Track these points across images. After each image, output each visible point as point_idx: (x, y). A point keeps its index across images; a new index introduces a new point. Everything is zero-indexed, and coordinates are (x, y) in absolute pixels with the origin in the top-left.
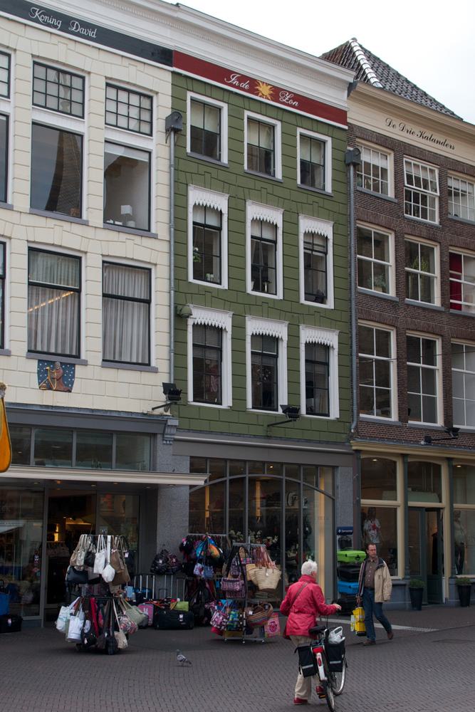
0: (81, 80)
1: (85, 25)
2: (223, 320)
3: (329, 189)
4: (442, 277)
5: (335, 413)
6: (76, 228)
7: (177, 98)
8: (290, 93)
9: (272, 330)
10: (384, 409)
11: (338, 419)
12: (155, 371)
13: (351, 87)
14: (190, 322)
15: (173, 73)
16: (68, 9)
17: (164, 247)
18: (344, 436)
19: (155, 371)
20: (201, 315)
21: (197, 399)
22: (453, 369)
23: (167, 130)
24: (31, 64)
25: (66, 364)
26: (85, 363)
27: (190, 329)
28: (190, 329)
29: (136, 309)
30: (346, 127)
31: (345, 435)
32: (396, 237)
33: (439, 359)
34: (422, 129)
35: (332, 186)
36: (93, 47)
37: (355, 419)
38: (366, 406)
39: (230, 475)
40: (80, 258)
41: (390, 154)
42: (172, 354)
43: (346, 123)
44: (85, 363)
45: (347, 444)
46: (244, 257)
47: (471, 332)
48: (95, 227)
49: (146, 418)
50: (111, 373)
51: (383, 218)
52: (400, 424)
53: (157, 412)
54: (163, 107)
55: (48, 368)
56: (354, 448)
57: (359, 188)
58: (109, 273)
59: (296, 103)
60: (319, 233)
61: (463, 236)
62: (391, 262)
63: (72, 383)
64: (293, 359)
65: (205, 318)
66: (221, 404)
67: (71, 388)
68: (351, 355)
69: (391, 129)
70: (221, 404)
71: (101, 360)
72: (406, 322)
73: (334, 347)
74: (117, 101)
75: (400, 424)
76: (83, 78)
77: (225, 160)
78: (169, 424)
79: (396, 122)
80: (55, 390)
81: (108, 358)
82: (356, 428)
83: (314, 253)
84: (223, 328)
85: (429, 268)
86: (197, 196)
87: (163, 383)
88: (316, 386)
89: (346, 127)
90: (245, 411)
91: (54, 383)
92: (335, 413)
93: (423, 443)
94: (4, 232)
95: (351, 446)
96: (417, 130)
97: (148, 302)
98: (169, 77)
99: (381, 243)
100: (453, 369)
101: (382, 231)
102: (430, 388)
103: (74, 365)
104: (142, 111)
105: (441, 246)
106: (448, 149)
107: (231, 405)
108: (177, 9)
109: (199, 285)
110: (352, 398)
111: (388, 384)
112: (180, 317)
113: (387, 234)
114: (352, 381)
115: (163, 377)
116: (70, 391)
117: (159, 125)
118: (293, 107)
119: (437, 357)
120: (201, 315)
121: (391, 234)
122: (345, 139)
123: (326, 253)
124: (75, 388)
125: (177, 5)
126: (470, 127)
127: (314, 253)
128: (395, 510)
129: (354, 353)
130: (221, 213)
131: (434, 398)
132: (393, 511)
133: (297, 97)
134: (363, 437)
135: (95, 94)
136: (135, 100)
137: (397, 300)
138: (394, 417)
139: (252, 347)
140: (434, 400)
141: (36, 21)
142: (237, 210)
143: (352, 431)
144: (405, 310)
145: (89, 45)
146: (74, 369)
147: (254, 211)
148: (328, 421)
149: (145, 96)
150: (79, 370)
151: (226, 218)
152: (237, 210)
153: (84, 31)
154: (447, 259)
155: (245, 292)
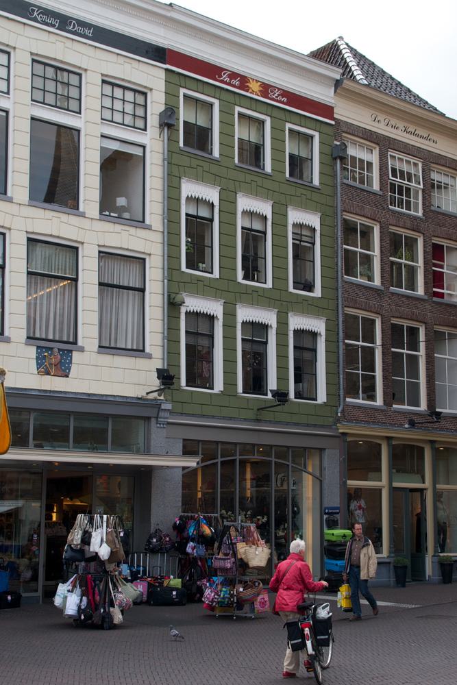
0: (78, 77)
1: (82, 24)
2: (214, 307)
3: (316, 182)
4: (425, 267)
5: (322, 397)
6: (74, 220)
7: (171, 94)
8: (279, 89)
9: (262, 318)
10: (370, 393)
11: (325, 403)
12: (149, 357)
13: (338, 84)
14: (183, 310)
15: (167, 70)
16: (66, 9)
17: (158, 238)
18: (331, 419)
19: (149, 357)
20: (193, 303)
21: (190, 384)
22: (436, 355)
23: (161, 126)
24: (30, 62)
25: (63, 350)
26: (82, 350)
27: (183, 317)
28: (183, 317)
29: (131, 298)
30: (333, 123)
31: (332, 419)
32: (381, 228)
33: (422, 346)
34: (406, 125)
35: (320, 179)
37: (342, 403)
38: (352, 391)
39: (221, 457)
40: (77, 248)
41: (375, 148)
42: (166, 340)
43: (333, 119)
44: (82, 350)
45: (334, 427)
46: (235, 247)
47: (453, 319)
48: (92, 219)
49: (140, 402)
50: (107, 359)
51: (368, 210)
52: (385, 408)
53: (151, 396)
54: (157, 103)
55: (46, 354)
56: (341, 431)
57: (345, 181)
58: (105, 262)
59: (285, 99)
60: (307, 224)
61: (445, 227)
62: (376, 252)
63: (69, 368)
64: (282, 346)
65: (197, 306)
66: (212, 389)
67: (69, 374)
68: (338, 342)
69: (376, 124)
70: (212, 389)
71: (97, 346)
73: (322, 334)
74: (113, 98)
75: (385, 408)
76: (80, 75)
77: (216, 154)
78: (163, 407)
79: (381, 117)
80: (53, 375)
81: (104, 344)
82: (343, 412)
83: (302, 243)
84: (215, 316)
85: (413, 257)
86: (189, 188)
87: (157, 369)
88: (304, 371)
89: (333, 123)
90: (235, 395)
91: (52, 369)
92: (322, 397)
93: (406, 426)
94: (4, 223)
95: (338, 429)
96: (401, 125)
97: (143, 290)
98: (162, 74)
99: (366, 233)
100: (436, 355)
101: (367, 222)
102: (414, 373)
103: (71, 351)
104: (137, 107)
105: (424, 236)
106: (431, 143)
107: (222, 390)
108: (170, 8)
109: (191, 274)
110: (339, 383)
111: (373, 369)
112: (173, 305)
113: (373, 225)
114: (338, 366)
115: (157, 363)
116: (67, 377)
117: (153, 121)
118: (282, 103)
119: (421, 343)
120: (193, 303)
121: (376, 225)
123: (314, 244)
124: (73, 373)
125: (171, 5)
126: (452, 123)
127: (302, 243)
128: (380, 491)
129: (341, 340)
130: (212, 205)
131: (418, 383)
132: (378, 491)
133: (285, 93)
135: (92, 91)
136: (129, 96)
138: (379, 401)
139: (243, 334)
140: (417, 385)
141: (35, 20)
142: (228, 202)
143: (339, 414)
144: (390, 298)
146: (72, 355)
147: (245, 203)
148: (316, 405)
149: (140, 92)
150: (76, 356)
151: (218, 210)
152: (228, 202)
153: (80, 30)
154: (430, 249)
155: (235, 281)
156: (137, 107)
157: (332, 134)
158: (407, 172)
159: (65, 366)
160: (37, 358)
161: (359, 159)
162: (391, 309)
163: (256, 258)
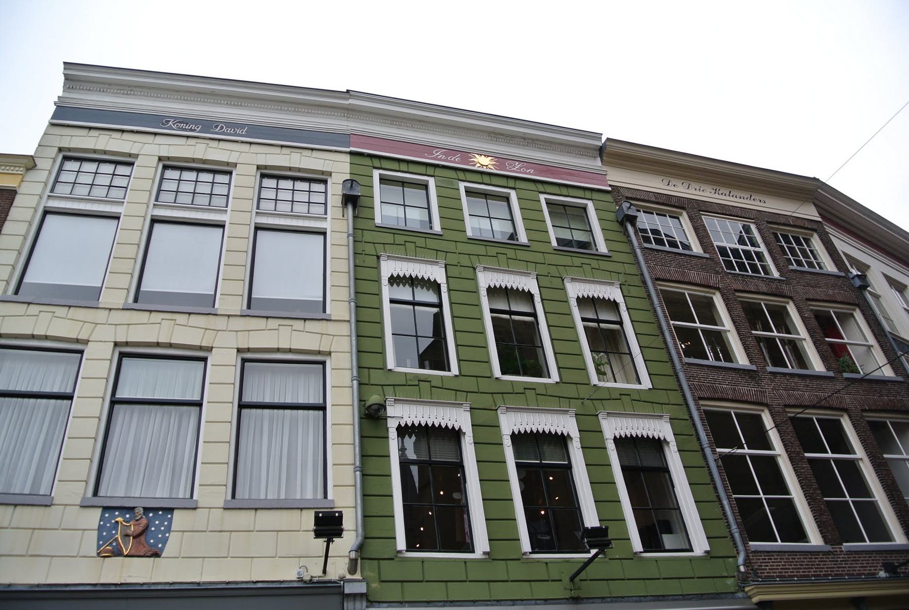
4: (812, 337)
5: (700, 545)
9: (635, 428)
11: (707, 552)
14: (392, 425)
15: (352, 153)
17: (345, 329)
18: (730, 581)
21: (536, 550)
22: (885, 456)
28: (393, 434)
30: (610, 189)
31: (732, 579)
32: (722, 296)
33: (774, 436)
36: (242, 142)
41: (812, 236)
42: (358, 473)
45: (740, 595)
47: (890, 400)
48: (229, 316)
55: (119, 519)
56: (755, 599)
57: (646, 245)
58: (851, 412)
60: (596, 296)
61: (820, 287)
64: (598, 465)
65: (635, 428)
67: (162, 549)
68: (703, 450)
73: (668, 440)
75: (829, 548)
78: (347, 591)
80: (127, 556)
82: (747, 562)
83: (602, 325)
84: (662, 439)
91: (126, 545)
93: (882, 574)
94: (158, 339)
95: (750, 598)
97: (323, 408)
101: (700, 292)
102: (859, 486)
105: (793, 301)
107: (488, 550)
108: (347, 96)
109: (512, 382)
110: (725, 514)
111: (867, 492)
113: (711, 295)
114: (715, 488)
116: (157, 555)
119: (770, 432)
121: (714, 294)
123: (620, 323)
125: (348, 91)
126: (786, 178)
129: (708, 451)
131: (872, 502)
134: (768, 580)
139: (517, 455)
140: (790, 503)
143: (742, 569)
144: (772, 381)
145: (237, 142)
146: (171, 519)
148: (690, 559)
151: (625, 309)
154: (739, 311)
155: (383, 368)
157: (612, 201)
161: (52, 118)
162: (780, 396)
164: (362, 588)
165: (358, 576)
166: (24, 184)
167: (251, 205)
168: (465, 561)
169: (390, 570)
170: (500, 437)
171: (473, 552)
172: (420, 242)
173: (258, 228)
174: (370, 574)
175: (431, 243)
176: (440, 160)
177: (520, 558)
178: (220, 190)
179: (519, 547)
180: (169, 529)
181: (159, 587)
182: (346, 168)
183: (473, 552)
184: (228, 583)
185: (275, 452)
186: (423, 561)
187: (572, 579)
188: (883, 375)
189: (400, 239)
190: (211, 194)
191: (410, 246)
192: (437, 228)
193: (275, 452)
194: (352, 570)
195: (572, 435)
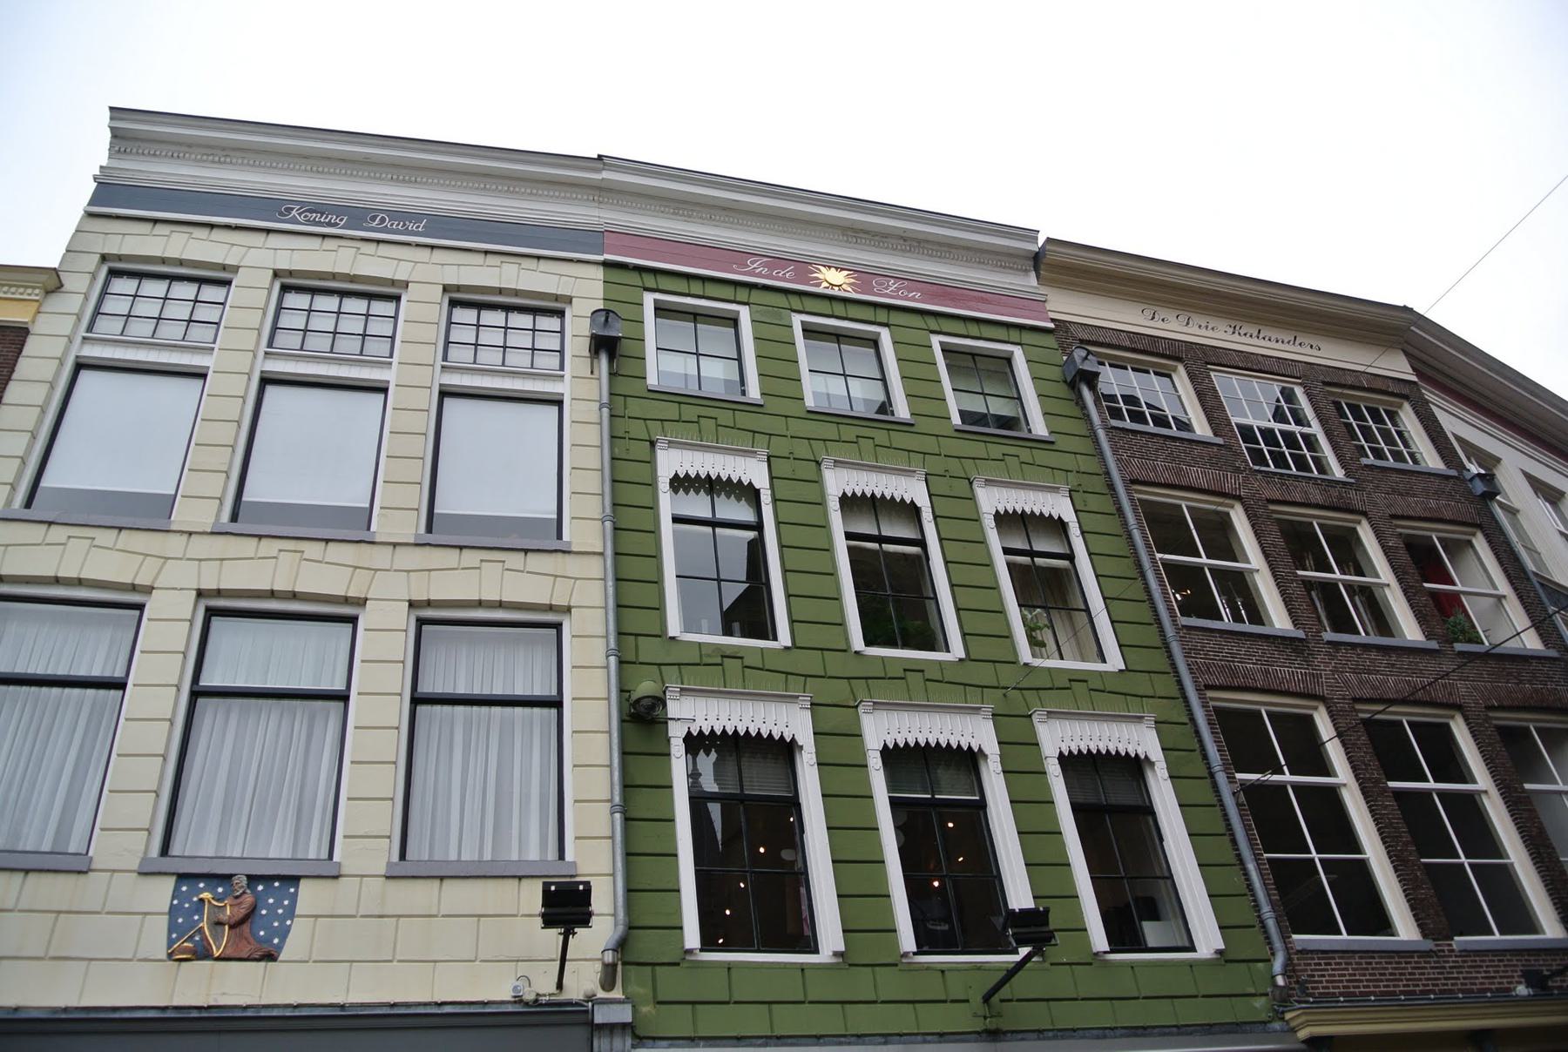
4: (1400, 580)
5: (1208, 939)
9: (1095, 738)
11: (1219, 952)
14: (677, 733)
15: (607, 265)
17: (594, 567)
18: (1259, 1003)
21: (925, 949)
22: (1527, 786)
28: (678, 748)
30: (1052, 325)
31: (1263, 999)
32: (1246, 510)
33: (1335, 752)
42: (618, 816)
45: (1277, 1025)
47: (1536, 691)
48: (395, 545)
55: (206, 895)
56: (1303, 1034)
57: (1115, 423)
58: (1468, 711)
60: (1028, 511)
61: (1414, 495)
64: (1031, 802)
65: (1095, 738)
67: (280, 947)
68: (1212, 775)
72: (1346, 682)
73: (1153, 759)
75: (1429, 945)
78: (598, 1019)
80: (219, 959)
82: (1289, 970)
83: (1039, 561)
84: (1143, 757)
91: (217, 939)
93: (1522, 990)
94: (272, 585)
95: (1293, 1030)
97: (557, 704)
101: (1208, 504)
102: (1481, 838)
105: (1368, 519)
107: (842, 948)
108: (599, 165)
109: (883, 658)
110: (1250, 887)
111: (1495, 849)
113: (1226, 509)
114: (1234, 842)
116: (270, 957)
119: (1328, 746)
121: (1232, 507)
122: (1056, 347)
123: (1070, 557)
125: (600, 157)
126: (1356, 306)
129: (1221, 778)
131: (1505, 865)
137: (1300, 634)
139: (892, 784)
140: (1363, 867)
143: (1280, 981)
144: (1332, 657)
146: (295, 896)
148: (1191, 965)
151: (1078, 532)
154: (1275, 537)
155: (661, 634)
156: (298, 337)
158: (1121, 395)
159: (278, 918)
160: (173, 911)
163: (1370, 607)
164: (624, 1014)
165: (617, 994)
166: (41, 318)
167: (433, 354)
168: (802, 968)
169: (673, 984)
170: (863, 753)
171: (816, 951)
172: (725, 417)
173: (445, 393)
174: (639, 990)
175: (744, 420)
176: (760, 275)
177: (897, 963)
178: (380, 327)
179: (896, 944)
180: (291, 913)
181: (275, 1013)
182: (598, 289)
183: (816, 951)
184: (394, 1005)
185: (475, 780)
186: (729, 967)
187: (987, 999)
188: (1522, 647)
189: (690, 412)
190: (364, 335)
191: (708, 424)
192: (754, 393)
193: (475, 780)
194: (608, 982)
195: (987, 750)
